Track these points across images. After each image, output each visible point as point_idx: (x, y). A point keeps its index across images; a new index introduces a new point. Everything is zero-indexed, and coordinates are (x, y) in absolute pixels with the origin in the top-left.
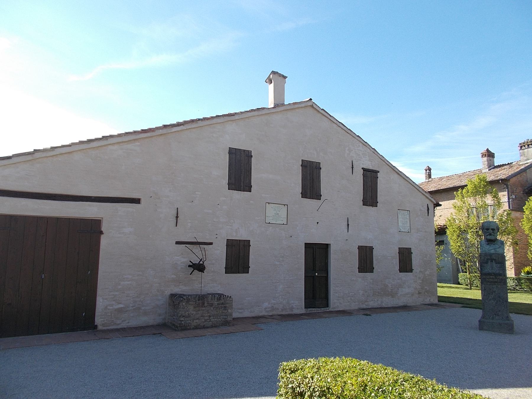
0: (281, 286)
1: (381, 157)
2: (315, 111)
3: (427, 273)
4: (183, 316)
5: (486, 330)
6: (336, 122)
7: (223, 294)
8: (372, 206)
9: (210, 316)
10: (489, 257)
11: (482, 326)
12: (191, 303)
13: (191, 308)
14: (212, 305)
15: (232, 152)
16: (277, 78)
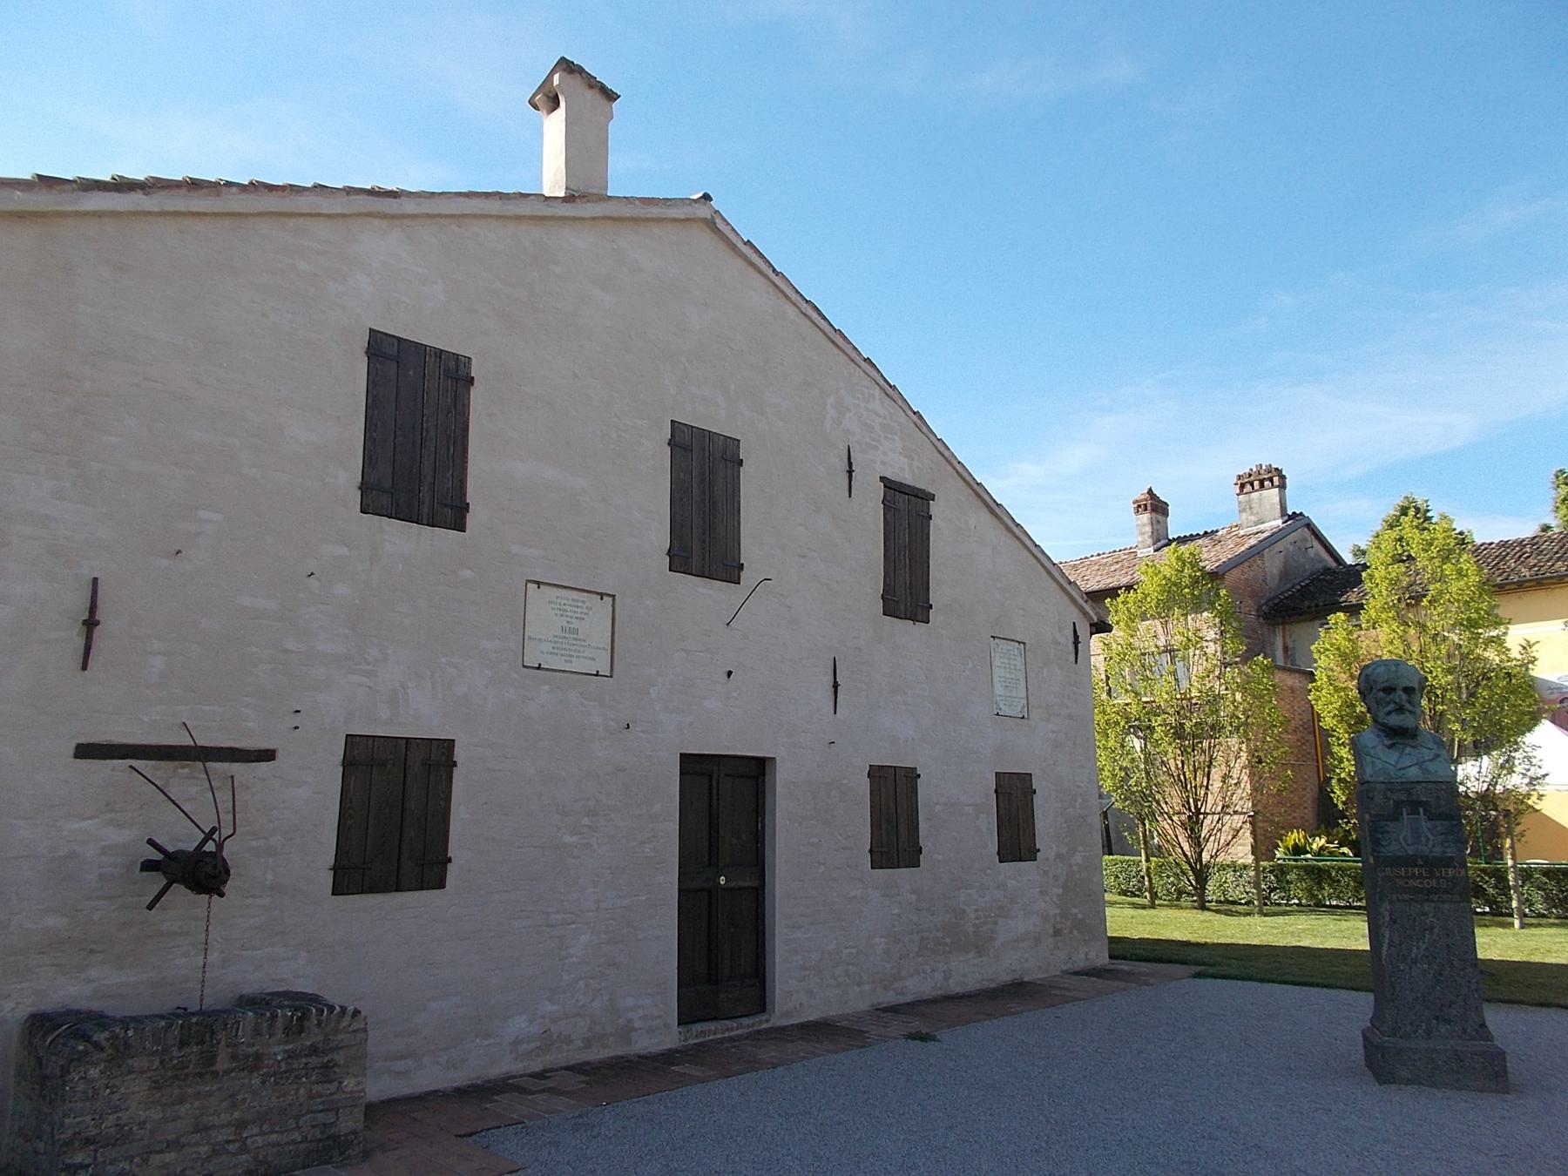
0: (584, 939)
1: (938, 444)
2: (721, 245)
3: (1078, 858)
4: (88, 1141)
5: (1408, 1082)
6: (794, 296)
7: (315, 999)
8: (914, 619)
9: (241, 1125)
10: (1403, 797)
11: (1382, 1061)
12: (136, 1063)
13: (136, 1089)
14: (254, 1063)
15: (385, 352)
16: (574, 87)
